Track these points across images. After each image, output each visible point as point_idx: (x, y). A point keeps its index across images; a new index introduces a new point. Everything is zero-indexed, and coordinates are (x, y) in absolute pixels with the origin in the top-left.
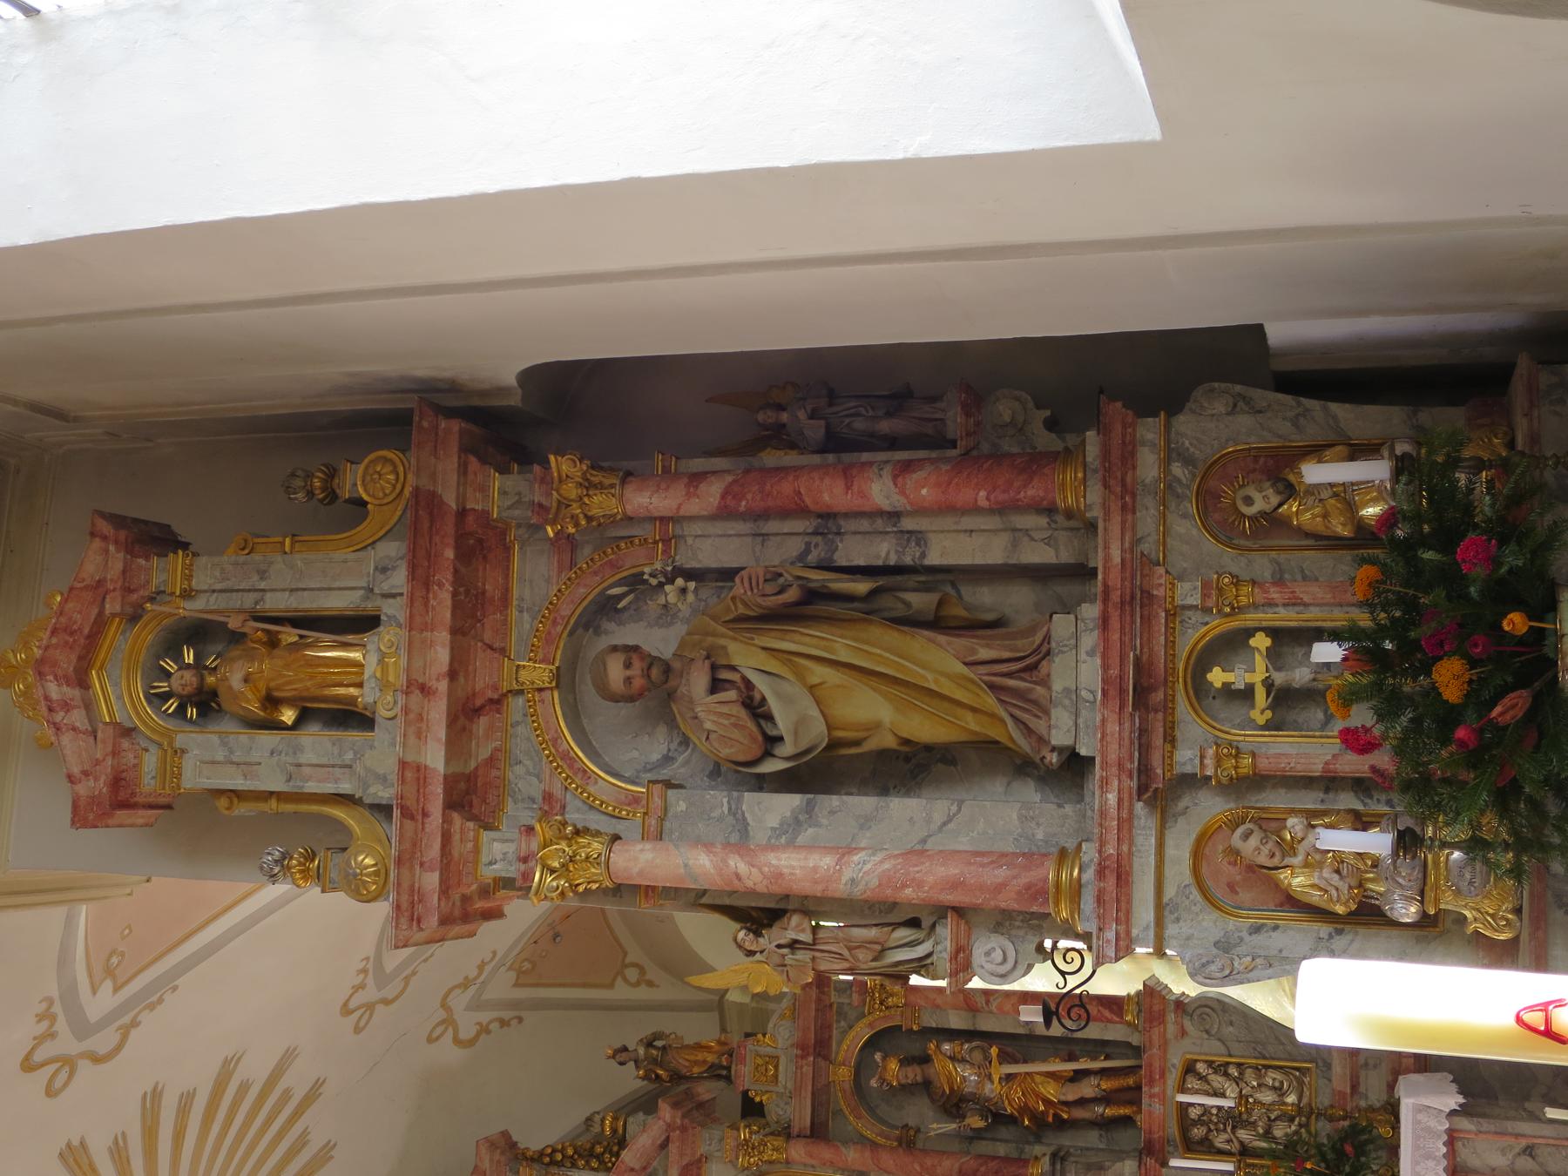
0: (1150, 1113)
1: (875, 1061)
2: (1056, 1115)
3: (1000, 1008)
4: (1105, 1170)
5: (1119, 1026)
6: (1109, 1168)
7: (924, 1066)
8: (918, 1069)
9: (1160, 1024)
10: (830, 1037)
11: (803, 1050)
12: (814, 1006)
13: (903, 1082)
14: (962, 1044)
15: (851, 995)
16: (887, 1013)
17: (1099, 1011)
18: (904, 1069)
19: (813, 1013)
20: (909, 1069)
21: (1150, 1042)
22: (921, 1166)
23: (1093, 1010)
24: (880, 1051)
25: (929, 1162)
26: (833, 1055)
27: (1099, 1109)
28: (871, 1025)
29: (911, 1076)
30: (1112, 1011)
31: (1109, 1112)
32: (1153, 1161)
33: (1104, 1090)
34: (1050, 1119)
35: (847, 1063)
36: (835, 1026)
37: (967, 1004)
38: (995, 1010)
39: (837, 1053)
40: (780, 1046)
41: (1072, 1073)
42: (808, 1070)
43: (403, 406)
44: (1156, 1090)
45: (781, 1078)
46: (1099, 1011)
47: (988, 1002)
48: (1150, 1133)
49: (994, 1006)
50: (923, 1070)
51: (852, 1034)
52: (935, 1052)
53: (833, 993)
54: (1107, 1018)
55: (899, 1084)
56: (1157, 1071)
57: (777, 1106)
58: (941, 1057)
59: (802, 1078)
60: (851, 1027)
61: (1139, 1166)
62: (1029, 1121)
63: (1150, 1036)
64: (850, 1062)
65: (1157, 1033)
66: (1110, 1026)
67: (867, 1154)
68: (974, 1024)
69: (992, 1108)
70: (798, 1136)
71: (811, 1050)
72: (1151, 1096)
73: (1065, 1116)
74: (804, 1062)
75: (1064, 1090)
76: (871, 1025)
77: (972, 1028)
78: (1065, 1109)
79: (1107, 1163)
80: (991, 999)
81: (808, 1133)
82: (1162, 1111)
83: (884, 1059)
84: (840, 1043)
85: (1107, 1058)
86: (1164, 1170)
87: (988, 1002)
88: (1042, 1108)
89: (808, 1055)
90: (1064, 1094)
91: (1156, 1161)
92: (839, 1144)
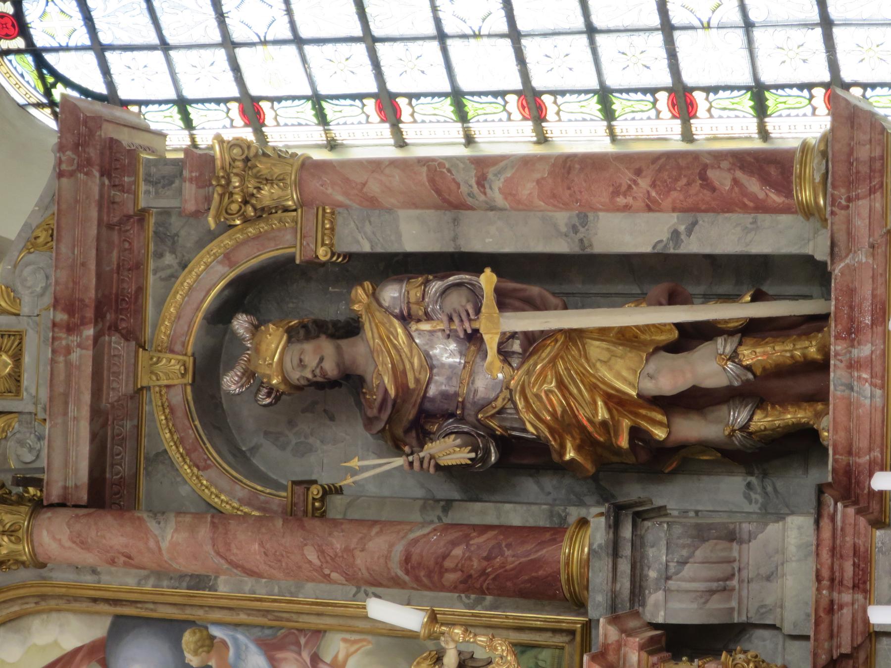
0: (850, 407)
1: (234, 334)
2: (636, 432)
3: (509, 192)
4: (741, 542)
5: (785, 218)
6: (751, 537)
7: (344, 343)
8: (327, 347)
9: (872, 191)
10: (141, 290)
11: (70, 309)
12: (94, 214)
13: (295, 376)
14: (426, 283)
15: (180, 191)
16: (263, 227)
17: (735, 181)
18: (296, 348)
19: (93, 231)
20: (308, 347)
21: (849, 233)
22: (321, 552)
23: (722, 179)
24: (246, 312)
25: (337, 543)
26: (149, 330)
27: (739, 416)
28: (228, 258)
29: (311, 361)
30: (766, 180)
31: (762, 421)
32: (851, 511)
33: (748, 368)
34: (624, 442)
35: (178, 347)
36: (152, 265)
37: (438, 192)
38: (499, 200)
39: (155, 326)
40: (25, 310)
41: (676, 334)
42: (82, 357)
43: (263, 468)
44: (865, 351)
45: (27, 380)
46: (735, 181)
47: (482, 181)
48: (850, 453)
49: (496, 185)
50: (338, 349)
51: (187, 280)
52: (368, 308)
53: (143, 187)
54: (754, 198)
55: (285, 380)
56: (867, 306)
57: (21, 443)
58: (378, 315)
59: (69, 377)
60: (184, 266)
61: (817, 522)
62: (579, 449)
63: (849, 221)
64: (184, 345)
65: (865, 213)
66: (765, 219)
67: (204, 532)
68: (455, 239)
69: (493, 424)
70: (62, 505)
71: (90, 314)
72: (853, 365)
73: (660, 434)
74: (74, 339)
75: (651, 367)
76: (228, 258)
77: (451, 249)
78: (660, 417)
79: (745, 526)
80: (491, 173)
81: (84, 497)
82: (878, 401)
83: (255, 329)
84: (161, 303)
85: (757, 297)
86: (878, 533)
87: (482, 181)
88: (602, 413)
89: (83, 323)
90: (650, 377)
91: (859, 512)
92: (145, 515)
